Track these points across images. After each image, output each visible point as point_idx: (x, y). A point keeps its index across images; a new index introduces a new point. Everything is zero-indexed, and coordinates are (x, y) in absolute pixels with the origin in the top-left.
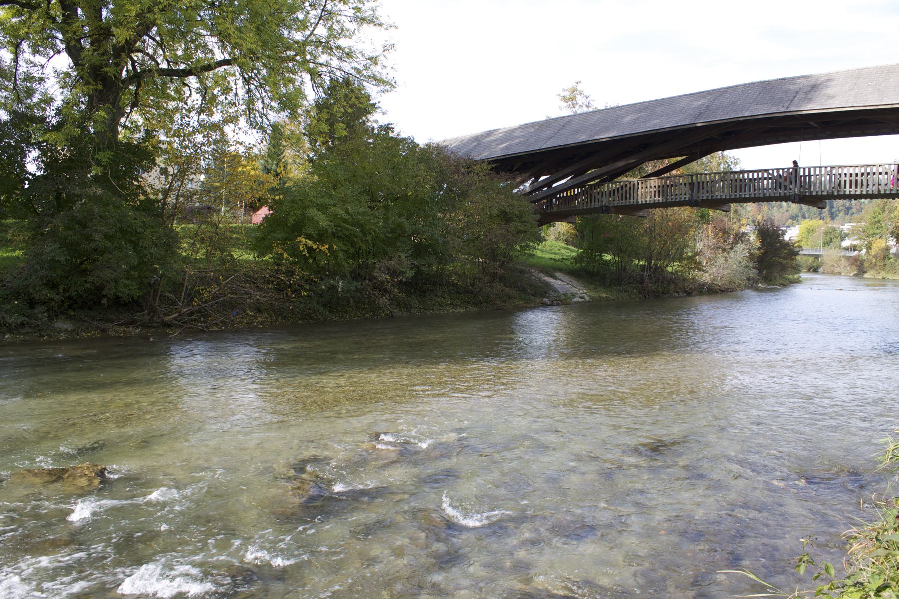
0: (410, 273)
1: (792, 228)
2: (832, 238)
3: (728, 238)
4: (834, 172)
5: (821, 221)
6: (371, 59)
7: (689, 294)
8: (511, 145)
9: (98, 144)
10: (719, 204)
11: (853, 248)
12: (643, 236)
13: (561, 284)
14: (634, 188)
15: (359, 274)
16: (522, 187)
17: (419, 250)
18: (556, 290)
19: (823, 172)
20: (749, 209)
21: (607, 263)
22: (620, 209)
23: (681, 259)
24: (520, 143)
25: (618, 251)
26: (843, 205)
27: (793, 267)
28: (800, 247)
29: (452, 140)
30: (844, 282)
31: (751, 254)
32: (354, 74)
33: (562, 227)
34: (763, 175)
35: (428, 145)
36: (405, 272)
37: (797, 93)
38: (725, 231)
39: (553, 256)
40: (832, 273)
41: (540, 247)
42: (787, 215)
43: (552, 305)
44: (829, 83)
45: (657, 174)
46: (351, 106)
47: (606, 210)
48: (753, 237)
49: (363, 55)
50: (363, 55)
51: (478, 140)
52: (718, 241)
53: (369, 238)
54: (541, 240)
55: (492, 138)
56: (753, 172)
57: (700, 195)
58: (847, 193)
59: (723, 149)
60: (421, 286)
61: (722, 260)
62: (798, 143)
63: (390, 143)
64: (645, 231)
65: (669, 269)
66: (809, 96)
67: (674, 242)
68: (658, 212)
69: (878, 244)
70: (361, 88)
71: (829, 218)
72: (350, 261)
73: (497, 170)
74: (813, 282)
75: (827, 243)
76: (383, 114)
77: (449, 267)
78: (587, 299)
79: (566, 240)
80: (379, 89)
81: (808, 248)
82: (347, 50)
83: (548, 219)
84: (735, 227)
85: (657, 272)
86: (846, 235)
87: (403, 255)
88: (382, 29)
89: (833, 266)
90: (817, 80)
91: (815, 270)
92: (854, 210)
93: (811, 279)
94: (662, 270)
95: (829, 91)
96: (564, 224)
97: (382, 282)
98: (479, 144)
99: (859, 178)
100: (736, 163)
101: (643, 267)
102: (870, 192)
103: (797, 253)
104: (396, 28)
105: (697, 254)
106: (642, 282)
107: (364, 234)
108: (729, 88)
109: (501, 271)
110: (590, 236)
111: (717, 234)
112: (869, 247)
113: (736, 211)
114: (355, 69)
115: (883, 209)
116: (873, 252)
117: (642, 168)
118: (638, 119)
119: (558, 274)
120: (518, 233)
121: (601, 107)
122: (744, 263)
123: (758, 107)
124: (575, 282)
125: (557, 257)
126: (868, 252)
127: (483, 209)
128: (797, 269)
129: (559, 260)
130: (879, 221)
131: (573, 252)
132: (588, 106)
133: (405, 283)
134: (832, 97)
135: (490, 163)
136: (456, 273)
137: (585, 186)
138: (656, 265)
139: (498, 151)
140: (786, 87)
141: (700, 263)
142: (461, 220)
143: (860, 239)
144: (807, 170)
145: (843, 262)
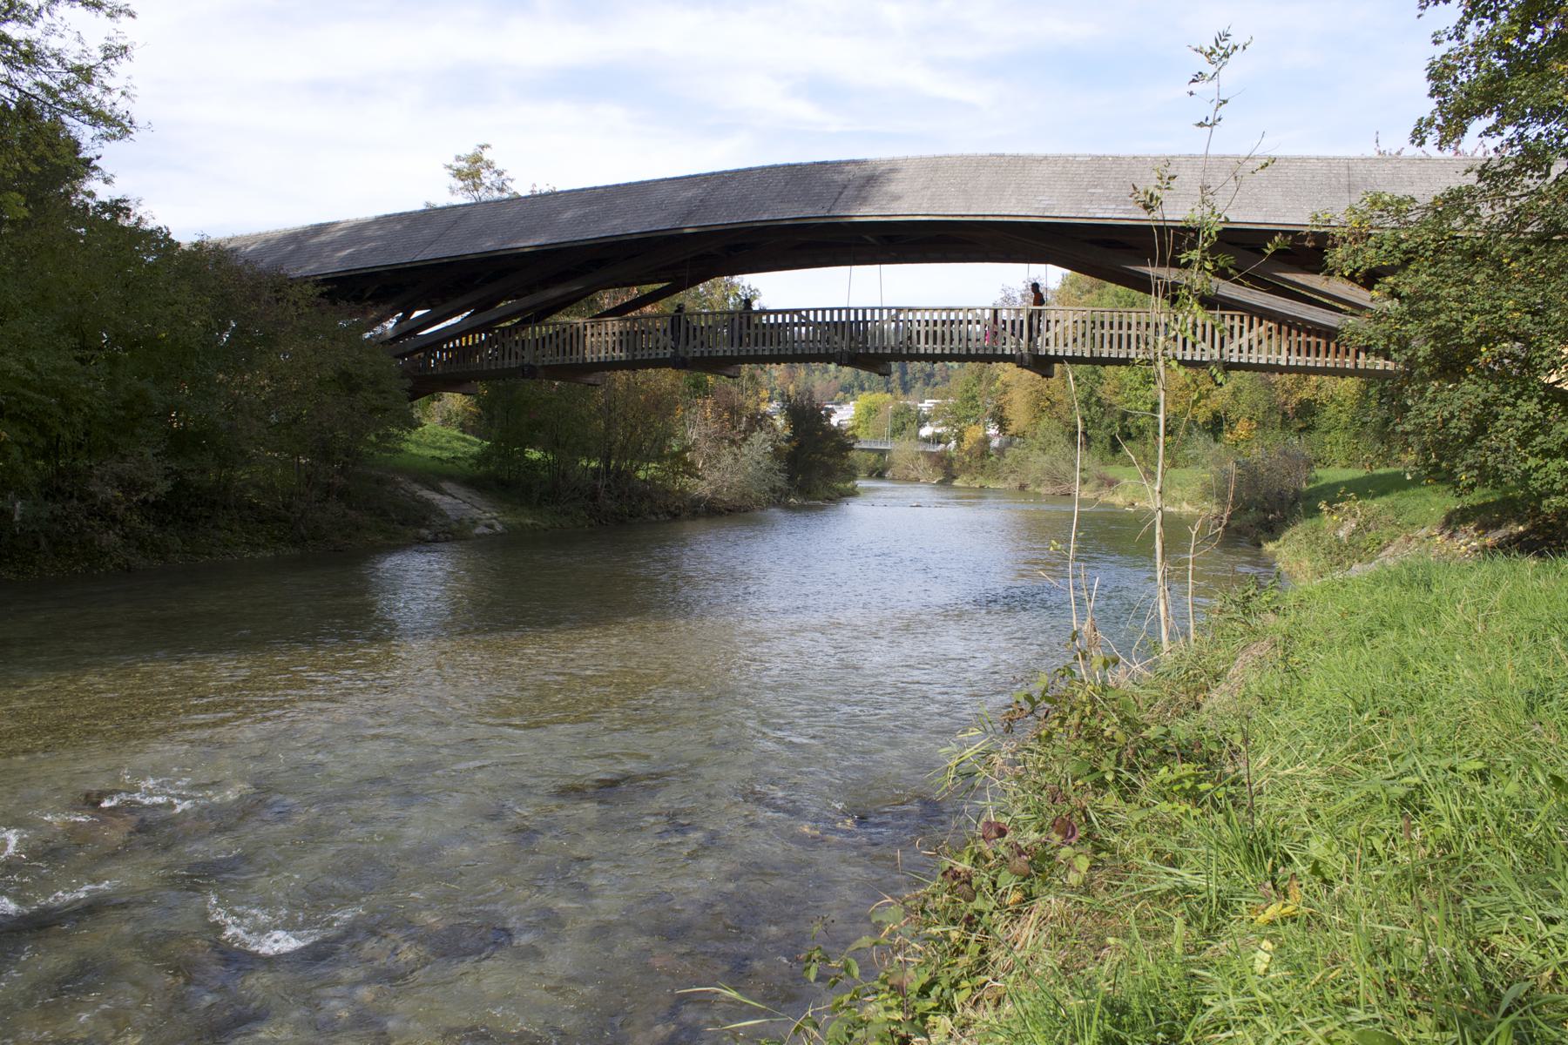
0: (163, 487)
1: (845, 407)
2: (906, 422)
3: (739, 422)
5: (888, 396)
6: (78, 70)
7: (675, 516)
8: (359, 252)
10: (723, 364)
11: (937, 439)
12: (595, 418)
13: (451, 502)
14: (576, 336)
15: (58, 489)
16: (378, 330)
17: (180, 444)
18: (441, 514)
20: (775, 373)
21: (533, 464)
22: (554, 372)
23: (660, 458)
24: (373, 250)
25: (552, 445)
26: (922, 370)
27: (844, 471)
28: (854, 437)
29: (247, 238)
30: (923, 493)
31: (776, 449)
32: (43, 96)
33: (454, 401)
34: (792, 318)
35: (199, 246)
36: (154, 484)
37: (845, 187)
38: (734, 411)
39: (437, 453)
40: (906, 480)
41: (414, 436)
42: (835, 384)
43: (435, 541)
44: (893, 175)
45: (619, 311)
46: (39, 161)
47: (530, 372)
48: (780, 422)
49: (60, 61)
50: (60, 61)
51: (299, 241)
52: (722, 428)
53: (77, 418)
54: (414, 424)
55: (323, 238)
57: (690, 348)
59: (732, 274)
60: (185, 509)
61: (729, 460)
62: (843, 271)
63: (122, 242)
64: (600, 409)
65: (641, 474)
66: (863, 194)
67: (649, 430)
68: (621, 376)
69: (974, 433)
70: (58, 126)
71: (899, 392)
72: (40, 463)
73: (331, 297)
75: (898, 431)
76: (107, 181)
77: (242, 474)
78: (499, 528)
79: (461, 425)
80: (97, 131)
82: (23, 47)
83: (427, 386)
84: (751, 403)
85: (621, 478)
86: (927, 418)
87: (148, 452)
88: (102, 15)
89: (907, 468)
91: (880, 475)
92: (938, 379)
93: (878, 489)
94: (629, 477)
95: (893, 188)
96: (458, 396)
97: (107, 505)
98: (299, 248)
101: (596, 471)
102: (955, 352)
104: (132, 15)
105: (687, 449)
106: (594, 497)
107: (68, 411)
108: (737, 171)
109: (339, 481)
110: (503, 419)
111: (720, 416)
112: (960, 439)
113: (752, 378)
114: (44, 87)
115: (979, 378)
116: (966, 446)
117: (593, 300)
118: (585, 216)
119: (446, 485)
120: (371, 412)
121: (524, 192)
122: (766, 463)
124: (477, 499)
125: (446, 455)
126: (958, 445)
127: (304, 368)
128: (851, 473)
129: (448, 461)
130: (973, 398)
131: (473, 446)
132: (501, 190)
133: (154, 505)
134: (897, 198)
135: (317, 284)
136: (256, 486)
137: (491, 330)
138: (618, 468)
139: (337, 262)
141: (692, 464)
142: (263, 388)
143: (947, 425)
145: (922, 461)
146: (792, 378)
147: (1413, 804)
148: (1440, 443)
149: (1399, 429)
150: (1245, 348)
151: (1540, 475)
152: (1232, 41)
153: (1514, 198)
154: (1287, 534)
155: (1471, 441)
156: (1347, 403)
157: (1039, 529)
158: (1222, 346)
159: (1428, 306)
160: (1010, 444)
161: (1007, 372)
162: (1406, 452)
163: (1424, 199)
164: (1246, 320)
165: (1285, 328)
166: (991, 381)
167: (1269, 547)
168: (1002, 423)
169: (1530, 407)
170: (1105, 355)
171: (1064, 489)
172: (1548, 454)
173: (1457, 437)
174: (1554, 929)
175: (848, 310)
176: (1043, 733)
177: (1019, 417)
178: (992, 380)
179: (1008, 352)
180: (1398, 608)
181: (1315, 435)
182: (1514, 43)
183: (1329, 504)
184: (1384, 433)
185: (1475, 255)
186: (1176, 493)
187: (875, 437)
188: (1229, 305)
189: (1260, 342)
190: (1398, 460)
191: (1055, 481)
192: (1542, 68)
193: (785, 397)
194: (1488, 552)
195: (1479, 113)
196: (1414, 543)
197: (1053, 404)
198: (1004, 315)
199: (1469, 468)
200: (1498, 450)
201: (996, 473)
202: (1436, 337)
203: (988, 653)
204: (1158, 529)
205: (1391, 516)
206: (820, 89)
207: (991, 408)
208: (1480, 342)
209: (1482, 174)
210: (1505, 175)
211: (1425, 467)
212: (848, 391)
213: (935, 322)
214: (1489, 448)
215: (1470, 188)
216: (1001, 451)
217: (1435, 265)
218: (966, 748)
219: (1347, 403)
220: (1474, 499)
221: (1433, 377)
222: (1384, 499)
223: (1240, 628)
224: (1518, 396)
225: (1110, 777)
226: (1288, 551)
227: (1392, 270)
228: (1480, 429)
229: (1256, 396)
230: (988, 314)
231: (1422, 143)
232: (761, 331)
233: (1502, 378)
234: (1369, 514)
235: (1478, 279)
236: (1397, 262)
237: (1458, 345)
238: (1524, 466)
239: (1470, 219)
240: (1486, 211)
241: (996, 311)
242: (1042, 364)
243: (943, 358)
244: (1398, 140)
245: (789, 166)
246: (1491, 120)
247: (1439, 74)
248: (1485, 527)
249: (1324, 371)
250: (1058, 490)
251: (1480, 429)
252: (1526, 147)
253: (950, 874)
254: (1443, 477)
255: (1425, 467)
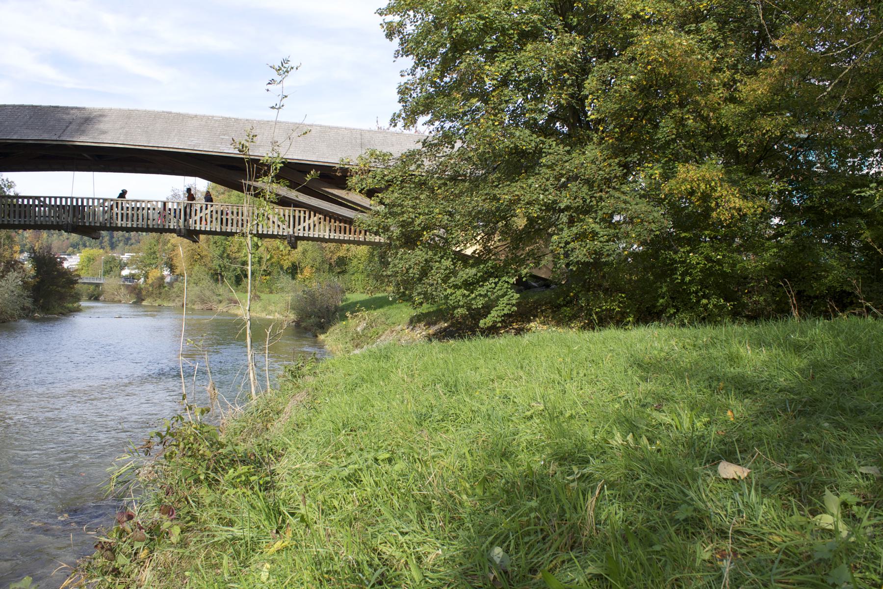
1: (74, 257)
2: (112, 267)
4: (106, 204)
5: (101, 251)
9: (621, 15)
11: (132, 277)
19: (96, 204)
26: (123, 236)
27: (72, 296)
28: (79, 276)
30: (123, 309)
31: (25, 283)
34: (34, 202)
37: (70, 123)
40: (113, 301)
42: (67, 242)
44: (101, 119)
48: (28, 265)
56: (29, 198)
58: (119, 225)
66: (83, 128)
69: (154, 274)
71: (108, 249)
74: (93, 310)
75: (107, 272)
81: (89, 276)
86: (126, 265)
89: (113, 294)
90: (90, 113)
92: (133, 241)
93: (93, 307)
95: (102, 126)
99: (145, 212)
100: (10, 187)
102: (140, 226)
103: (76, 282)
115: (158, 241)
123: (29, 131)
126: (145, 281)
128: (77, 298)
130: (154, 253)
140: (60, 115)
143: (138, 268)
144: (80, 201)
145: (123, 290)
146: (38, 238)
147: (354, 479)
148: (405, 281)
149: (385, 273)
150: (307, 228)
151: (453, 297)
152: (291, 64)
153: (440, 158)
154: (331, 330)
155: (420, 280)
156: (363, 259)
157: (193, 330)
158: (294, 227)
159: (398, 210)
160: (176, 280)
161: (173, 238)
162: (389, 286)
163: (397, 155)
164: (307, 213)
165: (328, 218)
166: (165, 243)
167: (322, 337)
168: (172, 268)
169: (447, 263)
170: (229, 230)
171: (208, 306)
172: (456, 287)
173: (413, 278)
174: (407, 537)
175: (72, 198)
176: (168, 454)
177: (182, 265)
178: (166, 243)
179: (172, 227)
180: (371, 372)
181: (347, 276)
182: (438, 81)
183: (352, 313)
184: (379, 278)
185: (422, 184)
186: (272, 308)
187: (93, 276)
188: (298, 204)
189: (315, 225)
190: (385, 290)
191: (203, 301)
192: (449, 95)
193: (32, 250)
194: (430, 338)
195: (422, 113)
196: (394, 334)
197: (202, 257)
198: (169, 205)
199: (419, 294)
200: (432, 285)
201: (168, 297)
202: (402, 226)
203: (160, 404)
204: (248, 331)
205: (383, 319)
206: (60, 60)
207: (165, 259)
208: (424, 229)
209: (424, 143)
210: (435, 145)
211: (398, 293)
212: (76, 247)
213: (138, 209)
214: (428, 284)
215: (419, 151)
216: (171, 284)
217: (401, 189)
218: (122, 464)
219: (363, 259)
220: (425, 308)
221: (401, 246)
222: (381, 310)
223: (291, 386)
224: (442, 257)
225: (202, 477)
226: (331, 339)
227: (380, 190)
228: (424, 273)
229: (315, 254)
230: (160, 205)
231: (395, 126)
232: (12, 209)
233: (434, 247)
234: (372, 318)
235: (422, 197)
236: (383, 186)
237: (413, 231)
238: (445, 293)
239: (419, 166)
240: (427, 163)
241: (165, 204)
242: (192, 235)
243: (131, 229)
244: (385, 123)
245: (33, 106)
246: (429, 117)
247: (403, 91)
248: (429, 324)
249: (349, 242)
250: (204, 306)
251: (424, 273)
252: (444, 132)
253: (100, 546)
254: (405, 298)
255: (398, 293)
